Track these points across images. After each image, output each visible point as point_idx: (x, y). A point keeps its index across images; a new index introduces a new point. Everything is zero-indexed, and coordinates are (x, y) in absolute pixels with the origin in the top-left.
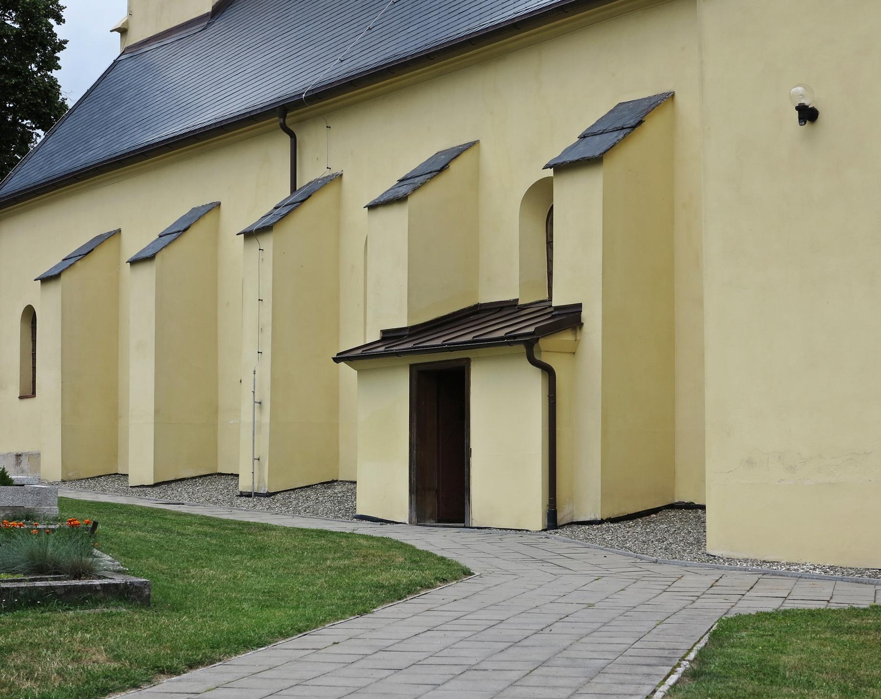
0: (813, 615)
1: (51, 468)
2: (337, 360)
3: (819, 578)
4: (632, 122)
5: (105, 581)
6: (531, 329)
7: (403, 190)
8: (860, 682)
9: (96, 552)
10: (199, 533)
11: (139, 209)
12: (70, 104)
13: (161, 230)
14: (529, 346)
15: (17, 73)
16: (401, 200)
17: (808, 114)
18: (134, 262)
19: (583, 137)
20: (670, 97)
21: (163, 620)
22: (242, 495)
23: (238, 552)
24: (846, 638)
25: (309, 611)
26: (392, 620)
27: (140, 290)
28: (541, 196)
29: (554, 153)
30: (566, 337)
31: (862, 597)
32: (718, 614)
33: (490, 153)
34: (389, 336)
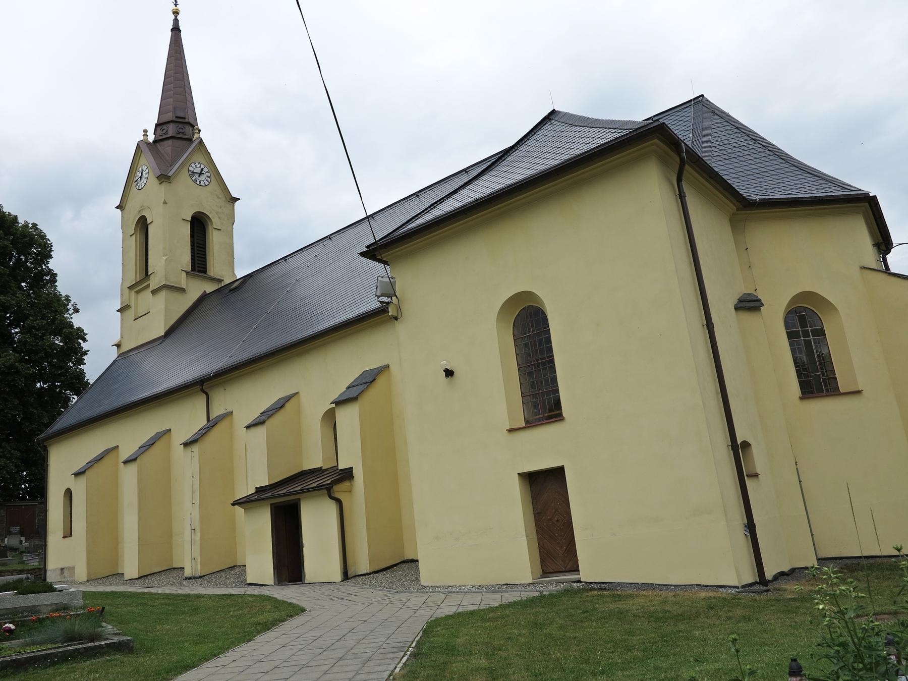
0: (472, 613)
1: (81, 573)
2: (233, 505)
3: (475, 592)
4: (370, 380)
5: (108, 642)
6: (329, 482)
7: (263, 418)
8: (494, 649)
9: (104, 624)
10: (162, 604)
11: (128, 436)
12: (91, 382)
13: (140, 444)
14: (328, 490)
15: (61, 368)
16: (263, 423)
17: (449, 373)
18: (125, 462)
19: (348, 388)
20: (387, 367)
21: (141, 660)
22: (186, 578)
23: (183, 613)
24: (488, 624)
25: (220, 644)
26: (266, 642)
27: (129, 477)
28: (330, 417)
29: (335, 396)
30: (346, 484)
31: (494, 600)
32: (426, 619)
33: (305, 398)
34: (259, 490)
